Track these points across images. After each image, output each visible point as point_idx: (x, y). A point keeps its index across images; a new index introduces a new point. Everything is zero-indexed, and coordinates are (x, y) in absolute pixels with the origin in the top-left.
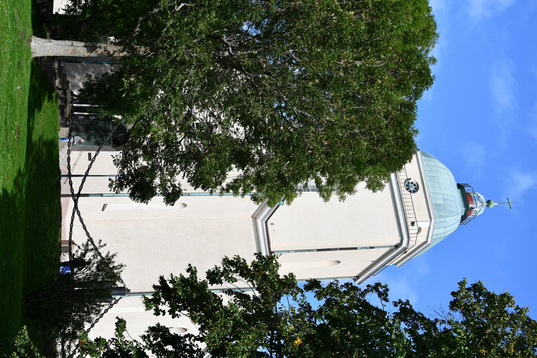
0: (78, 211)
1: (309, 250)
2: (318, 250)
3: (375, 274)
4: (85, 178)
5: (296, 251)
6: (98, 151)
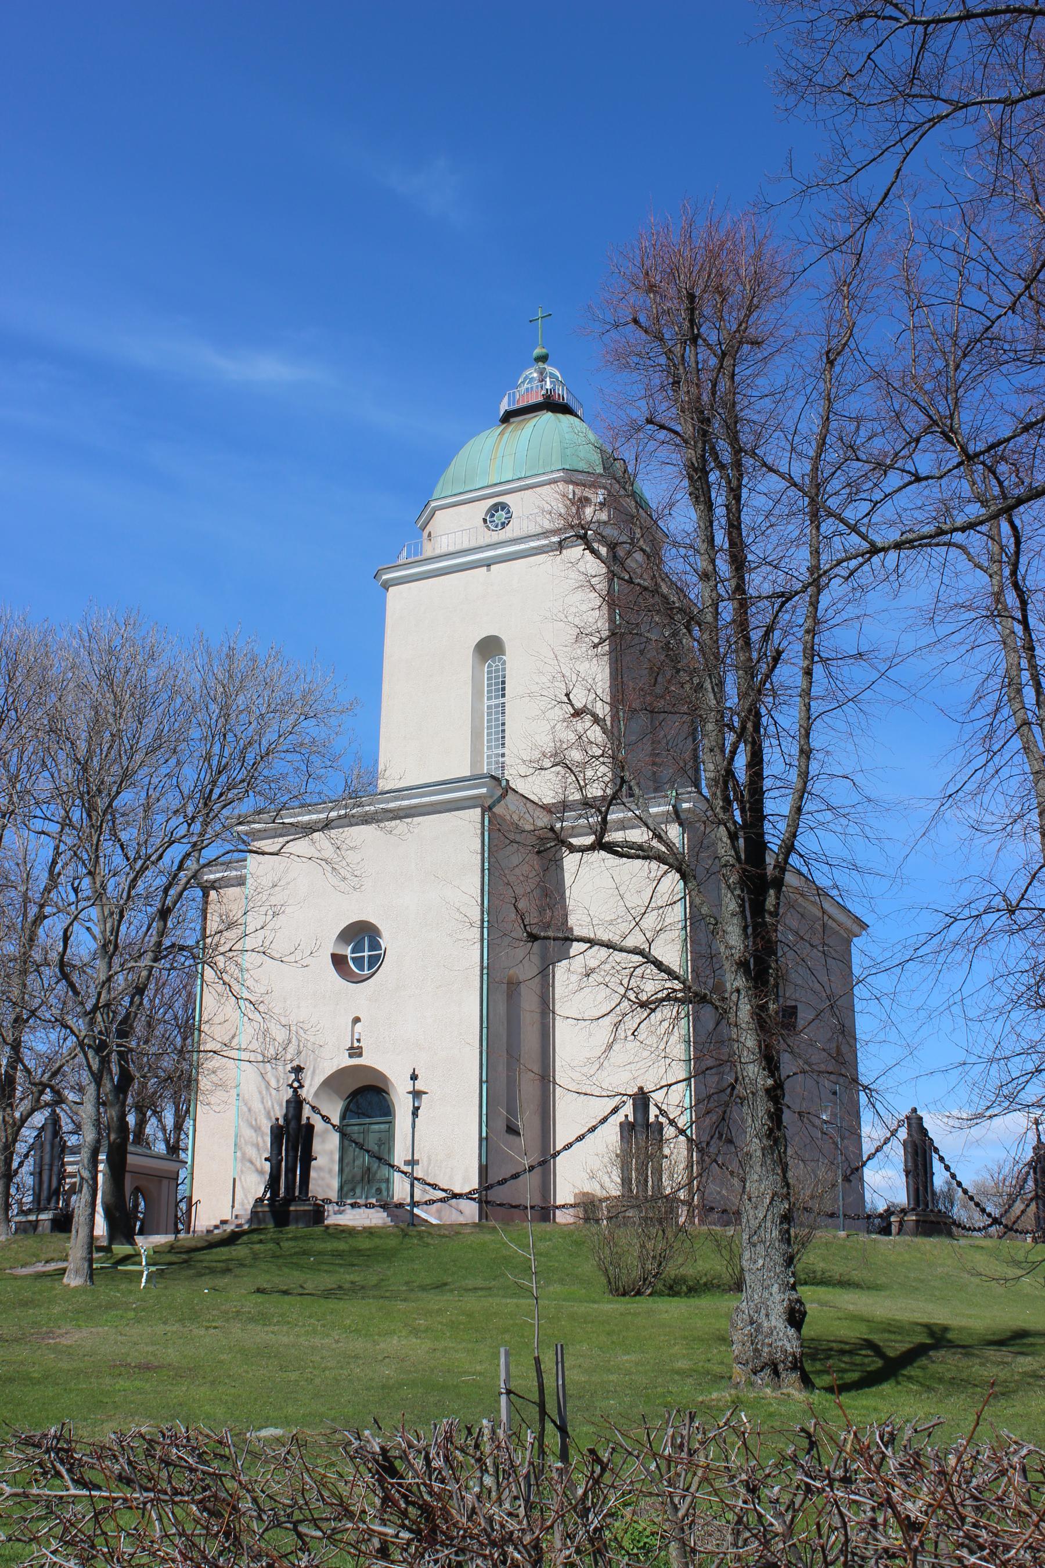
4: (416, 1179)
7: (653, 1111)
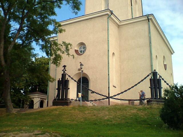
0: (114, 96)
1: (132, 9)
2: (132, 6)
5: (132, 14)
6: (90, 90)
7: (158, 76)
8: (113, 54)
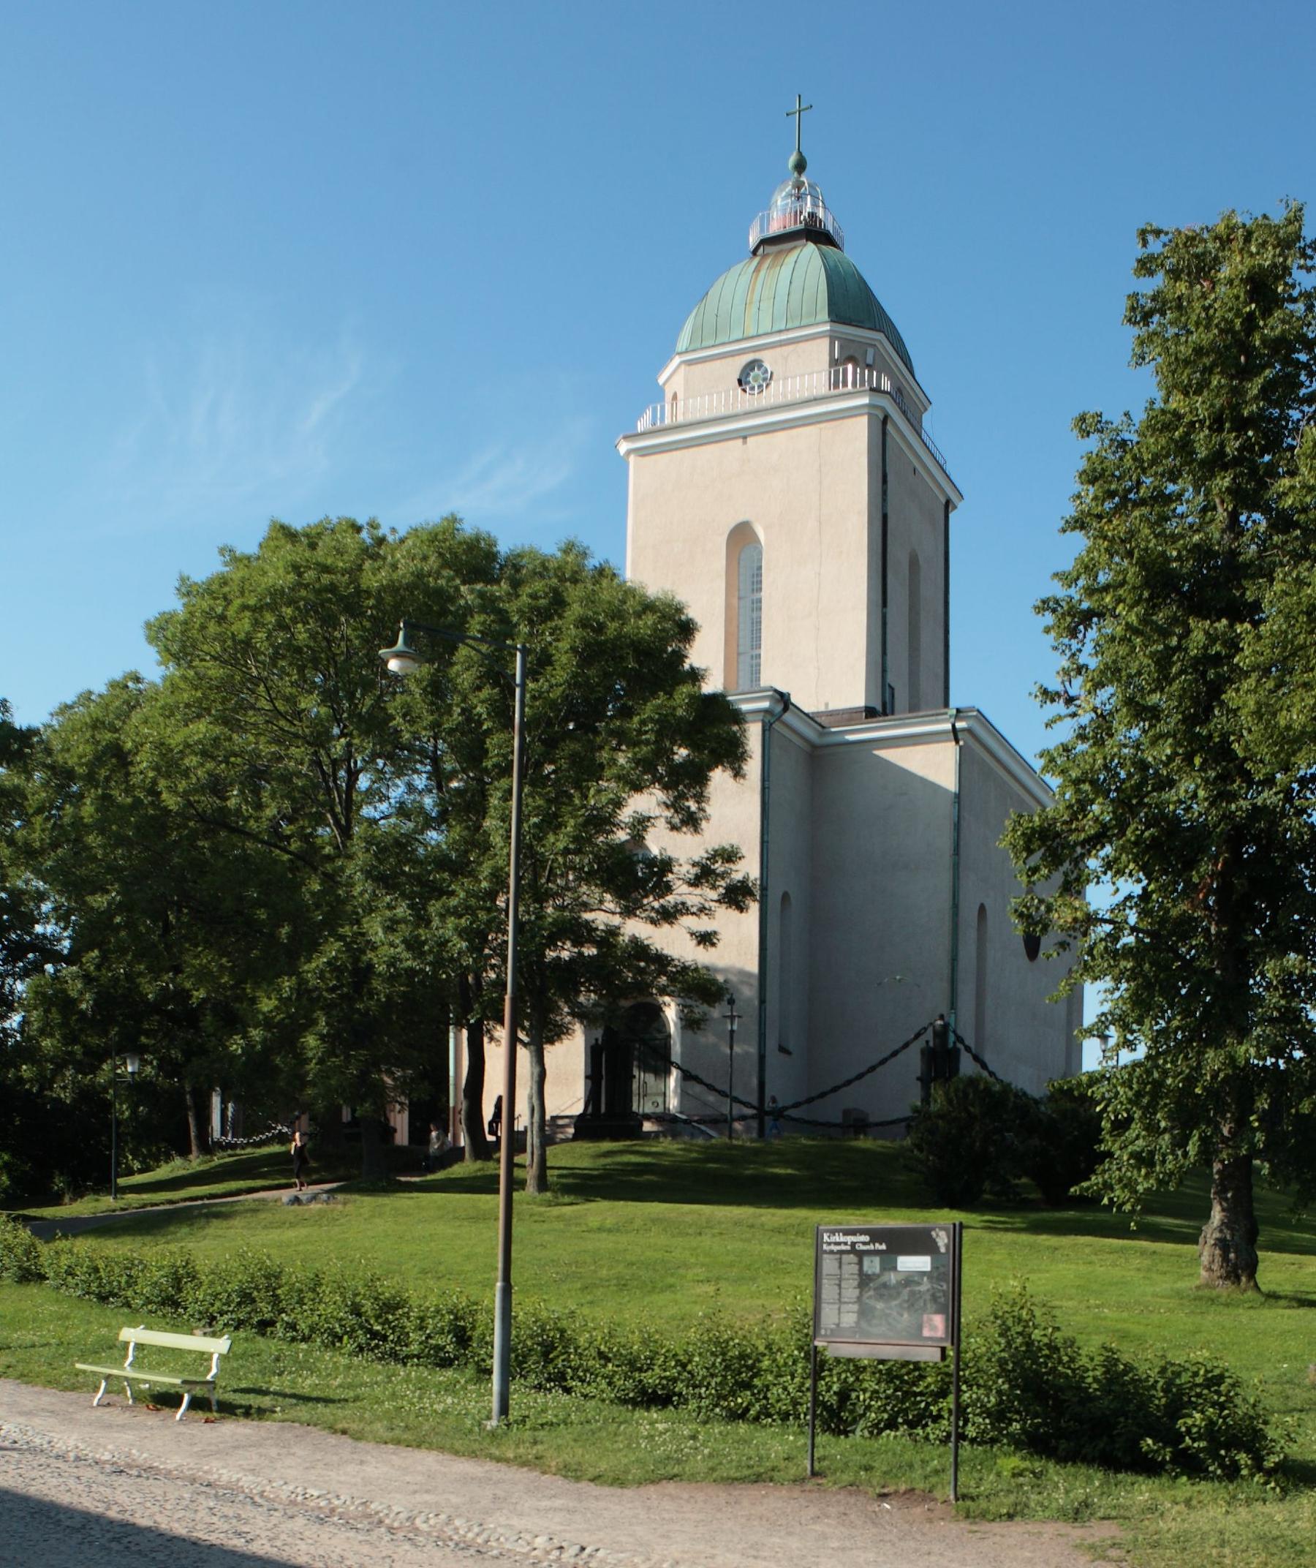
3: (942, 462)
7: (952, 1038)
8: (785, 896)
